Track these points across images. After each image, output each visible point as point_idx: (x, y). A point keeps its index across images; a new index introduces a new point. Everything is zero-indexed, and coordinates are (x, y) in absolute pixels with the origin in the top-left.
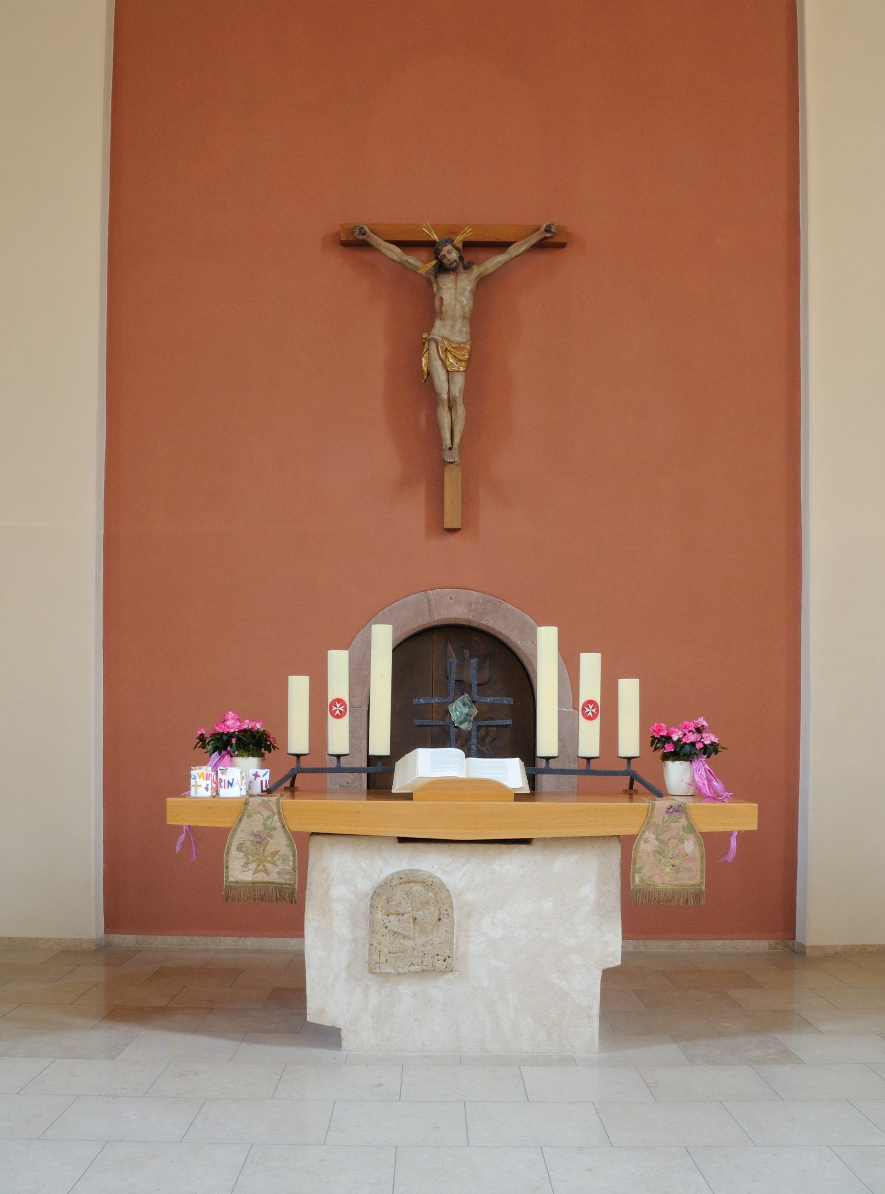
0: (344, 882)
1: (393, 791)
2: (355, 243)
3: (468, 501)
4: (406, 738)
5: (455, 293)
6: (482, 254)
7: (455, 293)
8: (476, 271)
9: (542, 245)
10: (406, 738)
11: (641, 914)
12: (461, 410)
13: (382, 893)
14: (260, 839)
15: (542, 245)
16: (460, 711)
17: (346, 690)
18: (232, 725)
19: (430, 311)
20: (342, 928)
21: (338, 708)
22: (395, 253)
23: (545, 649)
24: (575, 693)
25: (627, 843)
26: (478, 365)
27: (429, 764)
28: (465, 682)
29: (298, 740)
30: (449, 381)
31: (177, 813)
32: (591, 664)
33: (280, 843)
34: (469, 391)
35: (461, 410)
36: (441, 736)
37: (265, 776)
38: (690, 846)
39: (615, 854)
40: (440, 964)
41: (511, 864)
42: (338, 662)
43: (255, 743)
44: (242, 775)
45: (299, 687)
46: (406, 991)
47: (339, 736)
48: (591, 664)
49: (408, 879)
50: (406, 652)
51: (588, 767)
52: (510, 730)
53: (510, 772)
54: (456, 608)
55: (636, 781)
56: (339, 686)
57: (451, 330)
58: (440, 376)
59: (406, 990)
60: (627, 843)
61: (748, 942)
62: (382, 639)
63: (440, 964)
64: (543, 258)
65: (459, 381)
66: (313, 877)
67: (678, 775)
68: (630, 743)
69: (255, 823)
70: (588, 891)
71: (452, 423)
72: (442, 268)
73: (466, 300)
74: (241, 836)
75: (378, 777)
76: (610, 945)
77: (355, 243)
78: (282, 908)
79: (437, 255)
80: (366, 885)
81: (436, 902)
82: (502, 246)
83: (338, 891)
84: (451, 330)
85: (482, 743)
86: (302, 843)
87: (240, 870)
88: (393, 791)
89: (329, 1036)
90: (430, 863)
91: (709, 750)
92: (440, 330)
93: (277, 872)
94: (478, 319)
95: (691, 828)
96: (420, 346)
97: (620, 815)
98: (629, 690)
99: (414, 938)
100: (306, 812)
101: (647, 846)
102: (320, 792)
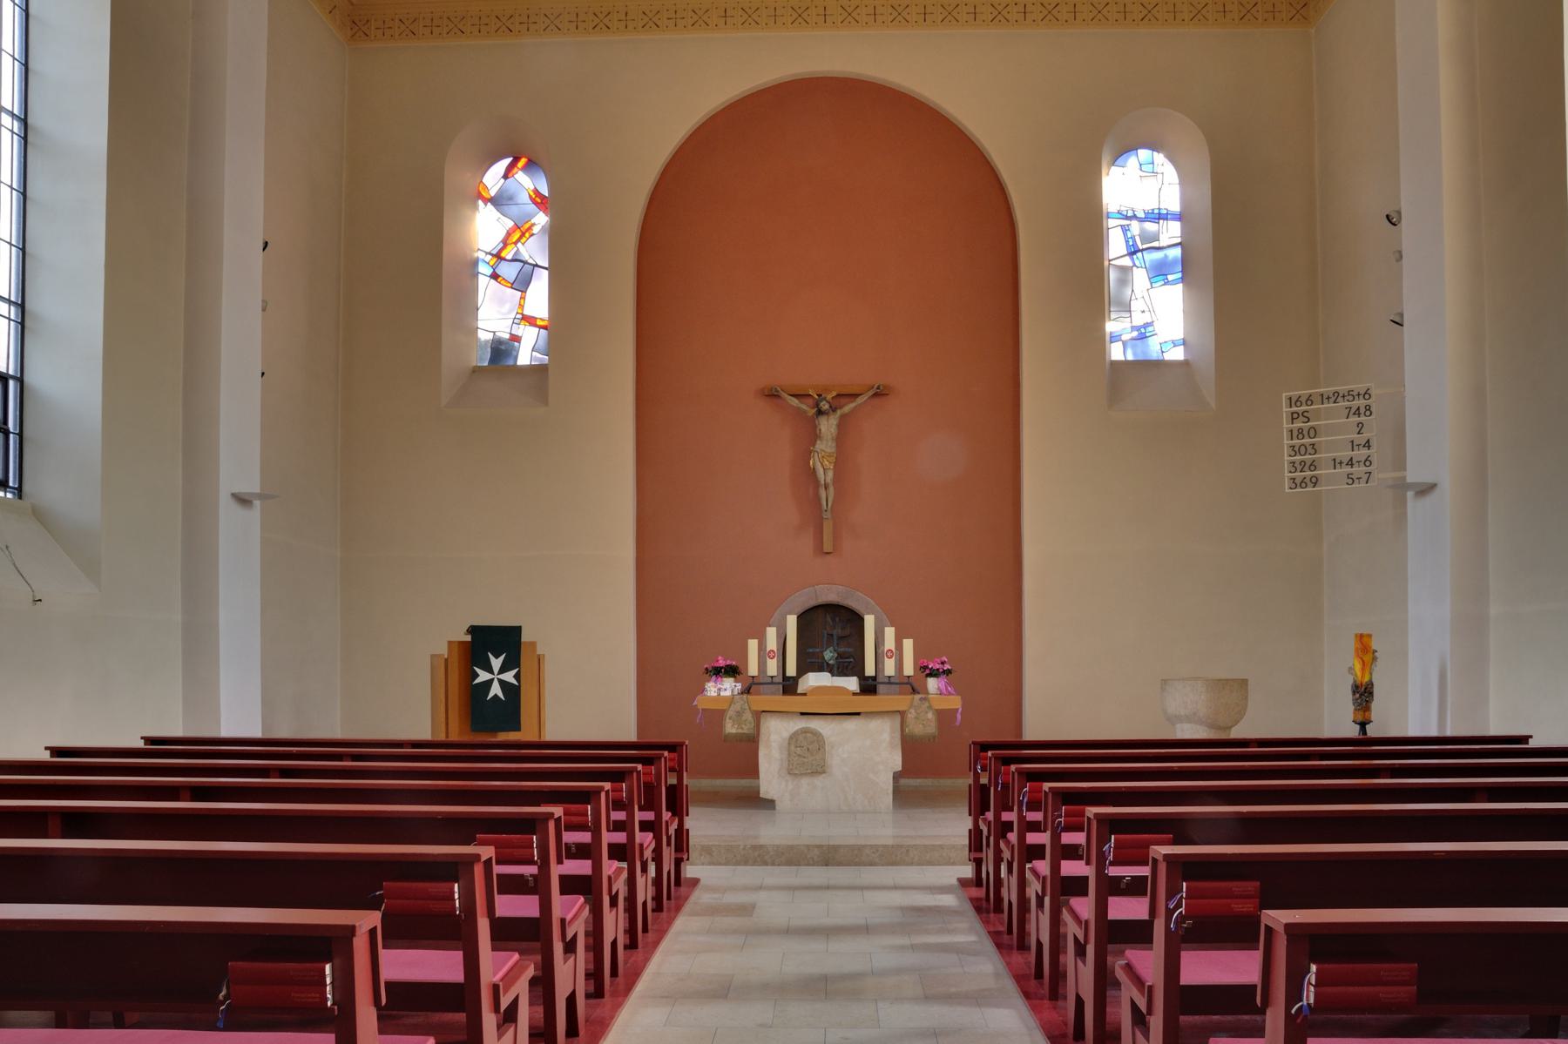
0: (777, 733)
1: (537, 914)
2: (772, 395)
3: (836, 537)
4: (803, 669)
5: (828, 426)
6: (843, 400)
7: (828, 426)
8: (839, 412)
9: (876, 395)
10: (803, 669)
11: (911, 747)
12: (831, 489)
13: (794, 737)
14: (739, 714)
15: (876, 395)
16: (829, 655)
17: (772, 645)
18: (722, 663)
19: (815, 436)
20: (776, 754)
21: (771, 655)
22: (794, 402)
23: (869, 622)
24: (888, 646)
25: (902, 714)
26: (841, 461)
27: (814, 680)
28: (831, 633)
29: (753, 670)
30: (825, 473)
31: (700, 703)
32: (890, 633)
33: (748, 716)
34: (837, 478)
35: (831, 489)
36: (820, 667)
37: (739, 686)
38: (930, 715)
39: (898, 719)
40: (819, 770)
41: (851, 724)
42: (771, 633)
43: (732, 671)
44: (729, 686)
45: (753, 645)
46: (805, 782)
47: (772, 668)
48: (890, 633)
49: (805, 731)
50: (805, 619)
51: (890, 681)
52: (850, 664)
53: (852, 683)
54: (831, 595)
55: (912, 687)
56: (772, 643)
57: (825, 446)
58: (820, 471)
59: (805, 781)
60: (902, 714)
61: (1332, 966)
62: (792, 622)
63: (819, 770)
64: (877, 401)
65: (830, 474)
66: (763, 730)
67: (932, 684)
68: (909, 670)
69: (737, 707)
70: (886, 736)
71: (827, 497)
72: (820, 413)
73: (834, 430)
74: (730, 713)
75: (789, 686)
76: (896, 761)
77: (772, 395)
78: (750, 742)
79: (817, 405)
80: (786, 735)
81: (818, 740)
82: (855, 396)
83: (773, 737)
84: (825, 446)
85: (841, 669)
86: (758, 715)
87: (730, 728)
88: (537, 914)
89: (770, 804)
90: (815, 724)
91: (948, 672)
92: (819, 446)
93: (747, 729)
94: (840, 439)
95: (930, 707)
96: (808, 454)
97: (901, 701)
98: (908, 644)
99: (808, 758)
100: (759, 701)
101: (911, 715)
102: (758, 693)
